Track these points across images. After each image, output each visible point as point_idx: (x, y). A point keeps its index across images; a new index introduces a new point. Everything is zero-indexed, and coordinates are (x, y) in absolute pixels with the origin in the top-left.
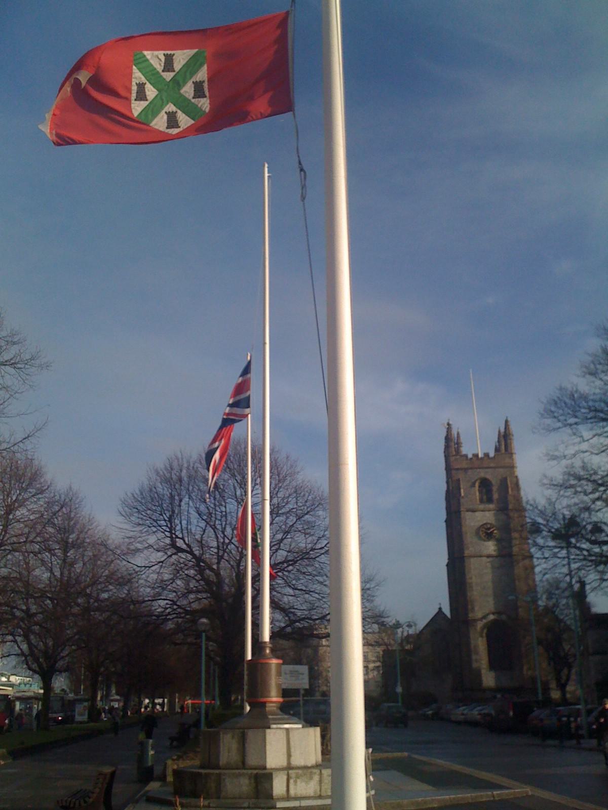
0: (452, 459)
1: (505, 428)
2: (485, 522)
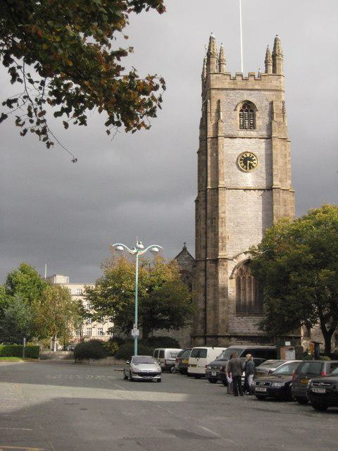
0: (213, 77)
1: (275, 48)
2: (244, 151)
